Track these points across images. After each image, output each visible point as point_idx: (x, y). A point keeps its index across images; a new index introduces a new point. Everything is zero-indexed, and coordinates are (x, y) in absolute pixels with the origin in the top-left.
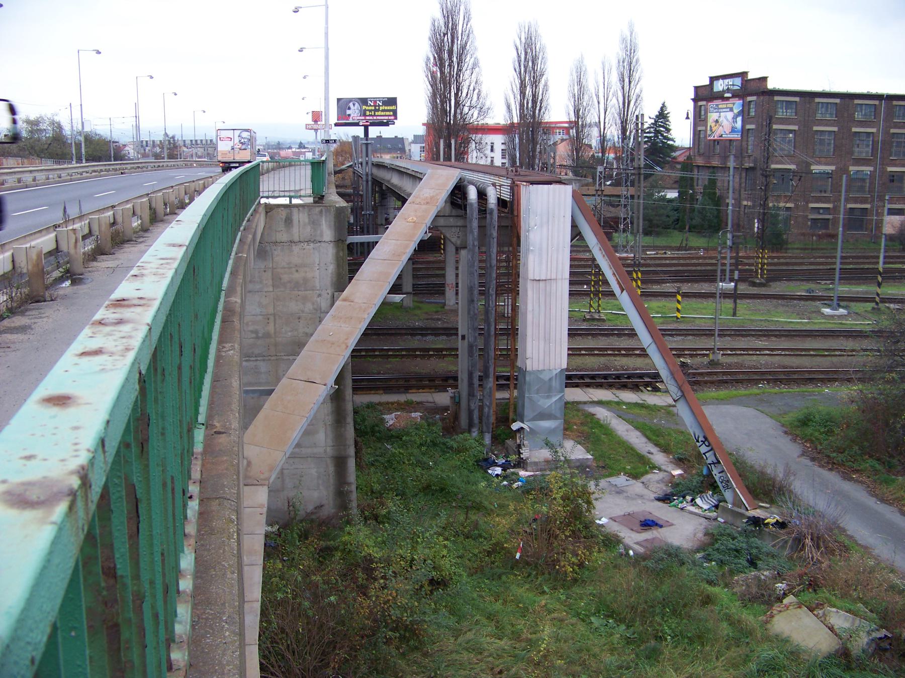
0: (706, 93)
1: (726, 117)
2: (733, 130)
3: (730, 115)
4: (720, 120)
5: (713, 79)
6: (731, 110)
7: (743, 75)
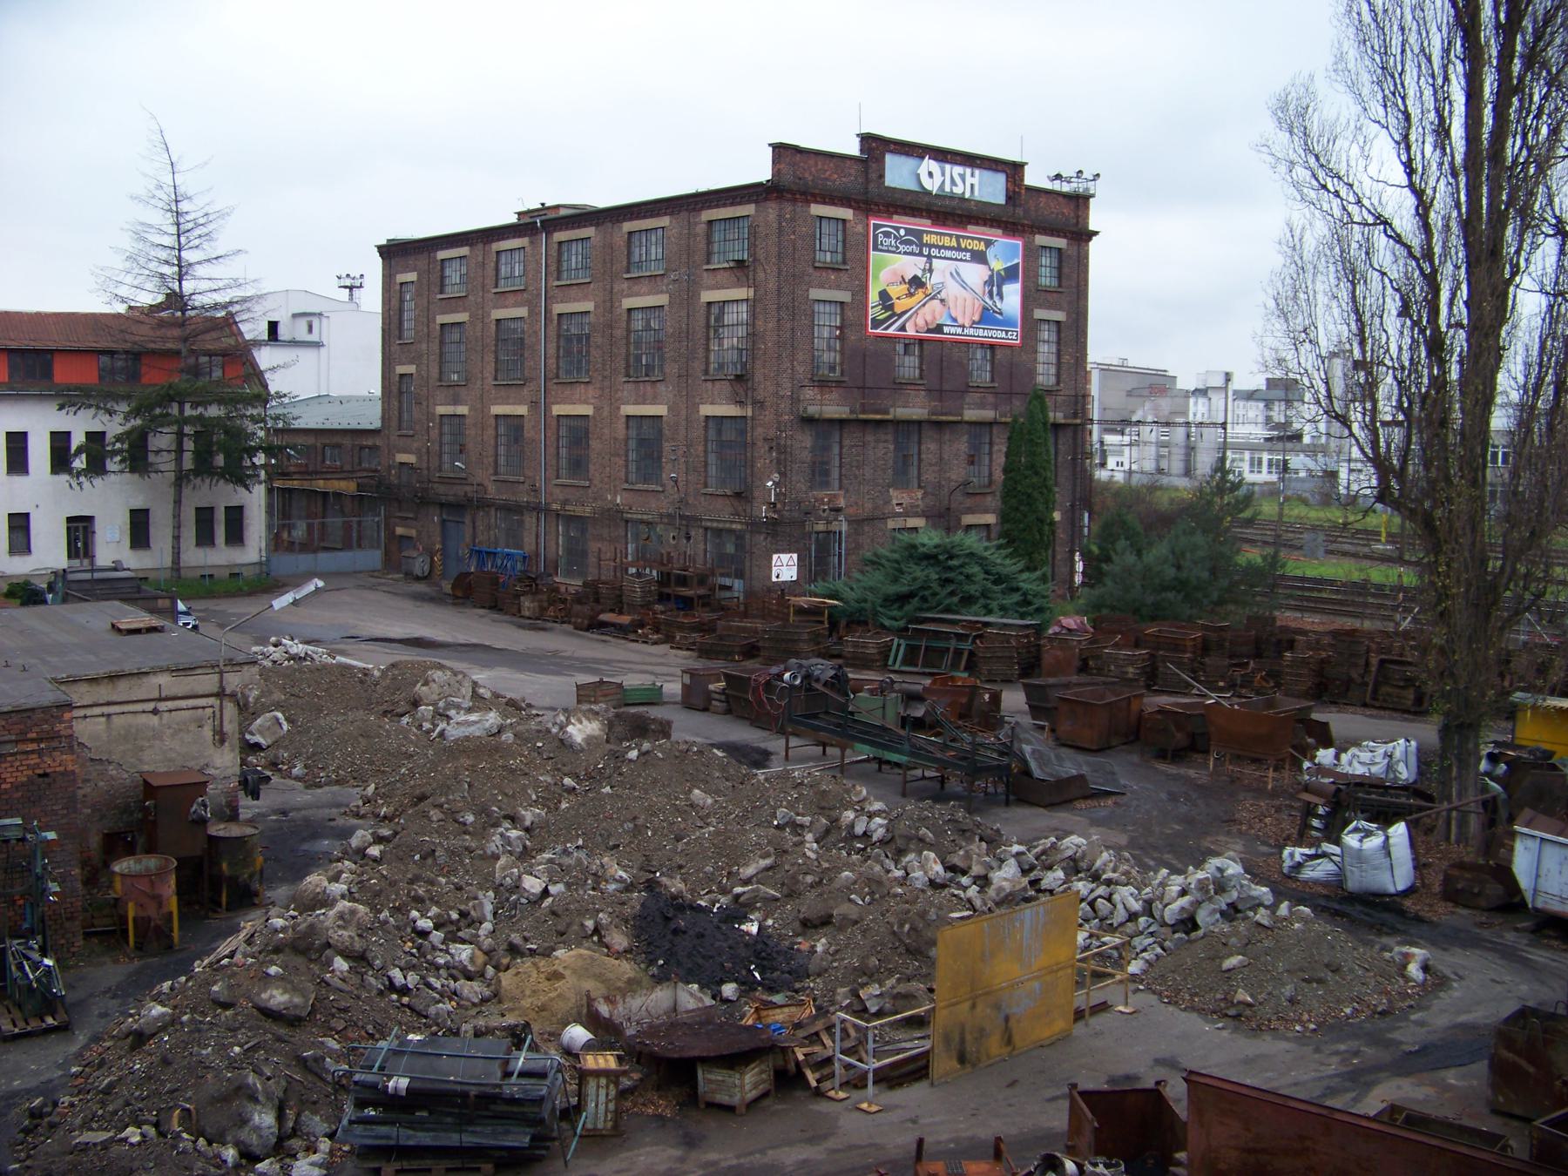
0: (848, 180)
1: (956, 275)
2: (988, 316)
3: (975, 274)
4: (934, 280)
5: (876, 146)
6: (979, 257)
7: (1014, 170)
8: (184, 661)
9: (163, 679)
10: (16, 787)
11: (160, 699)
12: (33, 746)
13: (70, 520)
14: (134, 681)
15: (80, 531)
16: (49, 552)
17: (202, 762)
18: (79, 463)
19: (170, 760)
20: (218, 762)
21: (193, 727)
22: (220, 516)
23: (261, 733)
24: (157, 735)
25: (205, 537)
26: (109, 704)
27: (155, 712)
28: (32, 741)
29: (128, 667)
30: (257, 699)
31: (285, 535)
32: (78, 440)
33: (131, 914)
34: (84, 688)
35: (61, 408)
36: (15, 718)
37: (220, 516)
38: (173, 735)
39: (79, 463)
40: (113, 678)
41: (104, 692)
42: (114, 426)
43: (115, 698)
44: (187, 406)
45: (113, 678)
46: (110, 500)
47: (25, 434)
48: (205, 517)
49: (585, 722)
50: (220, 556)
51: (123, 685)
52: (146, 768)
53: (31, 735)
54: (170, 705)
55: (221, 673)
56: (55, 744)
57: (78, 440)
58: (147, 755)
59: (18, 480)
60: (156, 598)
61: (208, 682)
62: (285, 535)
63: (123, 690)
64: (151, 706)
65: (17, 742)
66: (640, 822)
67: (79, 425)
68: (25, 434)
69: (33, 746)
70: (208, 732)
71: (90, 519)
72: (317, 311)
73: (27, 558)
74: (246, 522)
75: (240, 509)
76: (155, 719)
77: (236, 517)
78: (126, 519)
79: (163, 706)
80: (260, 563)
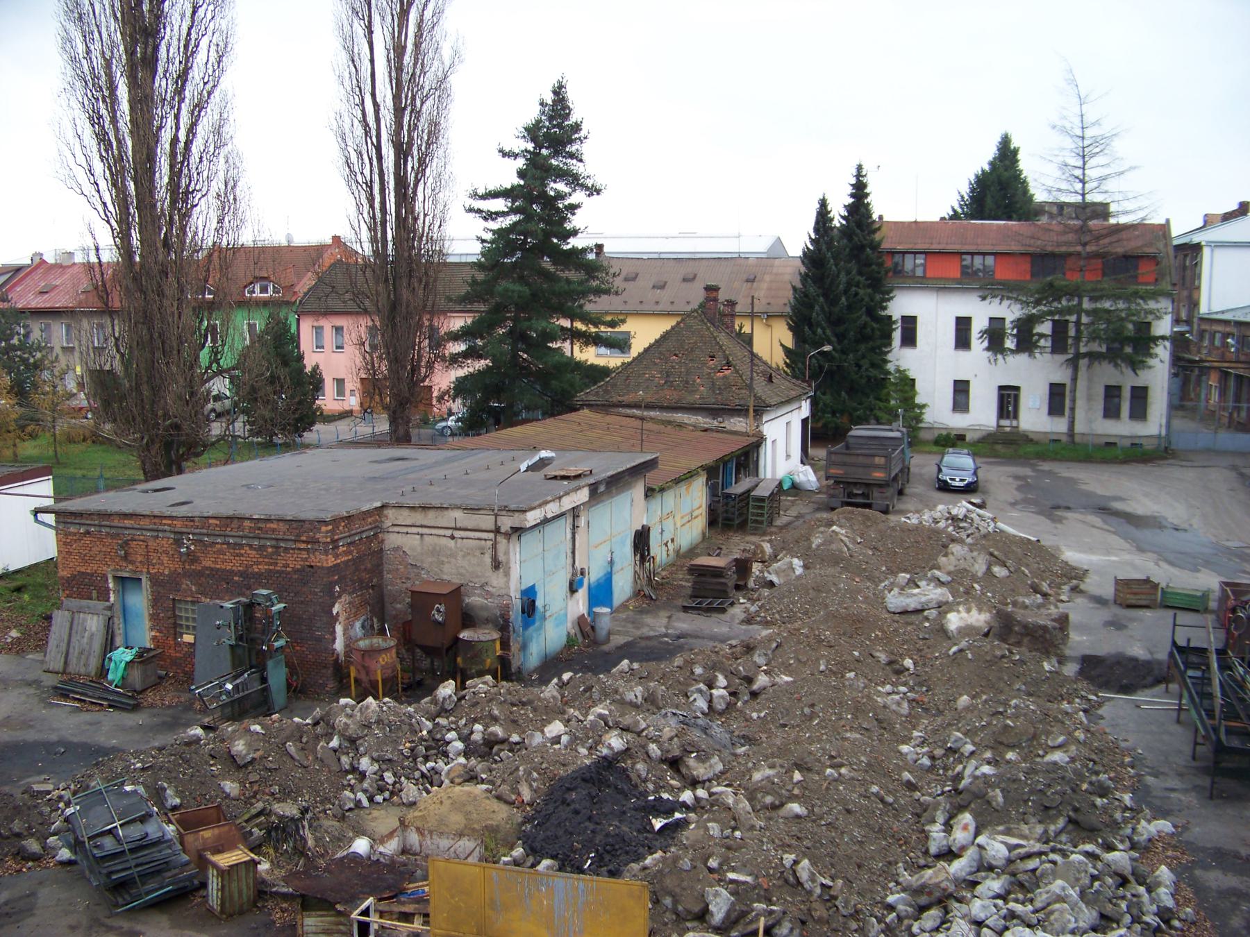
8: (472, 503)
9: (458, 514)
10: (296, 571)
11: (456, 529)
12: (303, 546)
13: (1001, 388)
14: (439, 512)
15: (1008, 399)
16: (982, 414)
17: (483, 580)
18: (1010, 343)
19: (461, 574)
20: (495, 583)
21: (478, 553)
22: (1126, 394)
23: (777, 573)
24: (453, 555)
25: (1111, 412)
26: (422, 526)
27: (452, 537)
28: (304, 542)
29: (436, 503)
30: (818, 546)
31: (1235, 415)
32: (979, 325)
33: (353, 675)
34: (406, 512)
35: (984, 298)
36: (295, 525)
37: (1126, 394)
38: (464, 556)
39: (1010, 343)
40: (425, 508)
41: (418, 518)
42: (1010, 312)
43: (425, 523)
44: (1085, 300)
45: (425, 508)
46: (1034, 374)
47: (970, 319)
48: (1112, 393)
49: (974, 612)
50: (1123, 428)
51: (431, 514)
52: (445, 577)
53: (304, 538)
54: (462, 534)
55: (496, 515)
56: (316, 547)
57: (979, 325)
58: (446, 568)
59: (962, 354)
60: (874, 456)
61: (487, 521)
62: (1235, 415)
63: (430, 518)
64: (449, 533)
65: (295, 541)
66: (817, 708)
67: (981, 312)
68: (970, 319)
69: (303, 546)
70: (488, 559)
71: (1017, 388)
72: (472, 215)
73: (965, 415)
74: (1150, 400)
75: (1145, 389)
76: (453, 542)
77: (1140, 395)
78: (1044, 391)
79: (457, 534)
80: (1159, 437)
